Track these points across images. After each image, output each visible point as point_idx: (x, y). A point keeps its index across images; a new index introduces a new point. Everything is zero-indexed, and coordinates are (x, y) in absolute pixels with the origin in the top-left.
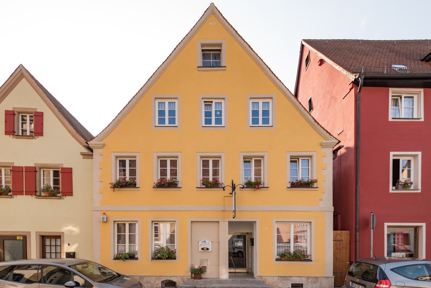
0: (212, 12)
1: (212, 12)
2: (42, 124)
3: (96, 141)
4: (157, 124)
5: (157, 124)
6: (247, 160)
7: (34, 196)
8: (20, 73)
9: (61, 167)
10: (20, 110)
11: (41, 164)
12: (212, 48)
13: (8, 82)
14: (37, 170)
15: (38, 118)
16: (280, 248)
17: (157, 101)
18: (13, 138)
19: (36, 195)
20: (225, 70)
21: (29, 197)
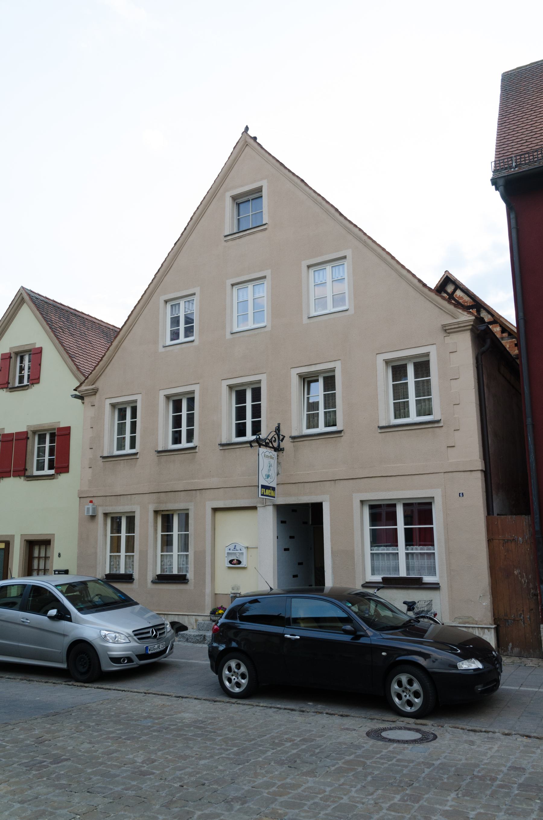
0: (247, 143)
1: (247, 143)
2: (40, 365)
3: (86, 386)
4: (169, 342)
5: (169, 342)
6: (308, 380)
7: (22, 478)
8: (20, 298)
9: (57, 426)
10: (17, 350)
11: (34, 426)
12: (252, 197)
13: (5, 317)
14: (29, 436)
15: (239, 201)
16: (413, 559)
17: (169, 306)
18: (6, 392)
19: (24, 476)
20: (265, 229)
21: (17, 479)
